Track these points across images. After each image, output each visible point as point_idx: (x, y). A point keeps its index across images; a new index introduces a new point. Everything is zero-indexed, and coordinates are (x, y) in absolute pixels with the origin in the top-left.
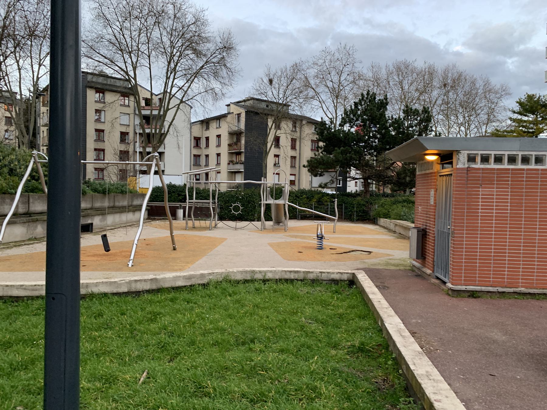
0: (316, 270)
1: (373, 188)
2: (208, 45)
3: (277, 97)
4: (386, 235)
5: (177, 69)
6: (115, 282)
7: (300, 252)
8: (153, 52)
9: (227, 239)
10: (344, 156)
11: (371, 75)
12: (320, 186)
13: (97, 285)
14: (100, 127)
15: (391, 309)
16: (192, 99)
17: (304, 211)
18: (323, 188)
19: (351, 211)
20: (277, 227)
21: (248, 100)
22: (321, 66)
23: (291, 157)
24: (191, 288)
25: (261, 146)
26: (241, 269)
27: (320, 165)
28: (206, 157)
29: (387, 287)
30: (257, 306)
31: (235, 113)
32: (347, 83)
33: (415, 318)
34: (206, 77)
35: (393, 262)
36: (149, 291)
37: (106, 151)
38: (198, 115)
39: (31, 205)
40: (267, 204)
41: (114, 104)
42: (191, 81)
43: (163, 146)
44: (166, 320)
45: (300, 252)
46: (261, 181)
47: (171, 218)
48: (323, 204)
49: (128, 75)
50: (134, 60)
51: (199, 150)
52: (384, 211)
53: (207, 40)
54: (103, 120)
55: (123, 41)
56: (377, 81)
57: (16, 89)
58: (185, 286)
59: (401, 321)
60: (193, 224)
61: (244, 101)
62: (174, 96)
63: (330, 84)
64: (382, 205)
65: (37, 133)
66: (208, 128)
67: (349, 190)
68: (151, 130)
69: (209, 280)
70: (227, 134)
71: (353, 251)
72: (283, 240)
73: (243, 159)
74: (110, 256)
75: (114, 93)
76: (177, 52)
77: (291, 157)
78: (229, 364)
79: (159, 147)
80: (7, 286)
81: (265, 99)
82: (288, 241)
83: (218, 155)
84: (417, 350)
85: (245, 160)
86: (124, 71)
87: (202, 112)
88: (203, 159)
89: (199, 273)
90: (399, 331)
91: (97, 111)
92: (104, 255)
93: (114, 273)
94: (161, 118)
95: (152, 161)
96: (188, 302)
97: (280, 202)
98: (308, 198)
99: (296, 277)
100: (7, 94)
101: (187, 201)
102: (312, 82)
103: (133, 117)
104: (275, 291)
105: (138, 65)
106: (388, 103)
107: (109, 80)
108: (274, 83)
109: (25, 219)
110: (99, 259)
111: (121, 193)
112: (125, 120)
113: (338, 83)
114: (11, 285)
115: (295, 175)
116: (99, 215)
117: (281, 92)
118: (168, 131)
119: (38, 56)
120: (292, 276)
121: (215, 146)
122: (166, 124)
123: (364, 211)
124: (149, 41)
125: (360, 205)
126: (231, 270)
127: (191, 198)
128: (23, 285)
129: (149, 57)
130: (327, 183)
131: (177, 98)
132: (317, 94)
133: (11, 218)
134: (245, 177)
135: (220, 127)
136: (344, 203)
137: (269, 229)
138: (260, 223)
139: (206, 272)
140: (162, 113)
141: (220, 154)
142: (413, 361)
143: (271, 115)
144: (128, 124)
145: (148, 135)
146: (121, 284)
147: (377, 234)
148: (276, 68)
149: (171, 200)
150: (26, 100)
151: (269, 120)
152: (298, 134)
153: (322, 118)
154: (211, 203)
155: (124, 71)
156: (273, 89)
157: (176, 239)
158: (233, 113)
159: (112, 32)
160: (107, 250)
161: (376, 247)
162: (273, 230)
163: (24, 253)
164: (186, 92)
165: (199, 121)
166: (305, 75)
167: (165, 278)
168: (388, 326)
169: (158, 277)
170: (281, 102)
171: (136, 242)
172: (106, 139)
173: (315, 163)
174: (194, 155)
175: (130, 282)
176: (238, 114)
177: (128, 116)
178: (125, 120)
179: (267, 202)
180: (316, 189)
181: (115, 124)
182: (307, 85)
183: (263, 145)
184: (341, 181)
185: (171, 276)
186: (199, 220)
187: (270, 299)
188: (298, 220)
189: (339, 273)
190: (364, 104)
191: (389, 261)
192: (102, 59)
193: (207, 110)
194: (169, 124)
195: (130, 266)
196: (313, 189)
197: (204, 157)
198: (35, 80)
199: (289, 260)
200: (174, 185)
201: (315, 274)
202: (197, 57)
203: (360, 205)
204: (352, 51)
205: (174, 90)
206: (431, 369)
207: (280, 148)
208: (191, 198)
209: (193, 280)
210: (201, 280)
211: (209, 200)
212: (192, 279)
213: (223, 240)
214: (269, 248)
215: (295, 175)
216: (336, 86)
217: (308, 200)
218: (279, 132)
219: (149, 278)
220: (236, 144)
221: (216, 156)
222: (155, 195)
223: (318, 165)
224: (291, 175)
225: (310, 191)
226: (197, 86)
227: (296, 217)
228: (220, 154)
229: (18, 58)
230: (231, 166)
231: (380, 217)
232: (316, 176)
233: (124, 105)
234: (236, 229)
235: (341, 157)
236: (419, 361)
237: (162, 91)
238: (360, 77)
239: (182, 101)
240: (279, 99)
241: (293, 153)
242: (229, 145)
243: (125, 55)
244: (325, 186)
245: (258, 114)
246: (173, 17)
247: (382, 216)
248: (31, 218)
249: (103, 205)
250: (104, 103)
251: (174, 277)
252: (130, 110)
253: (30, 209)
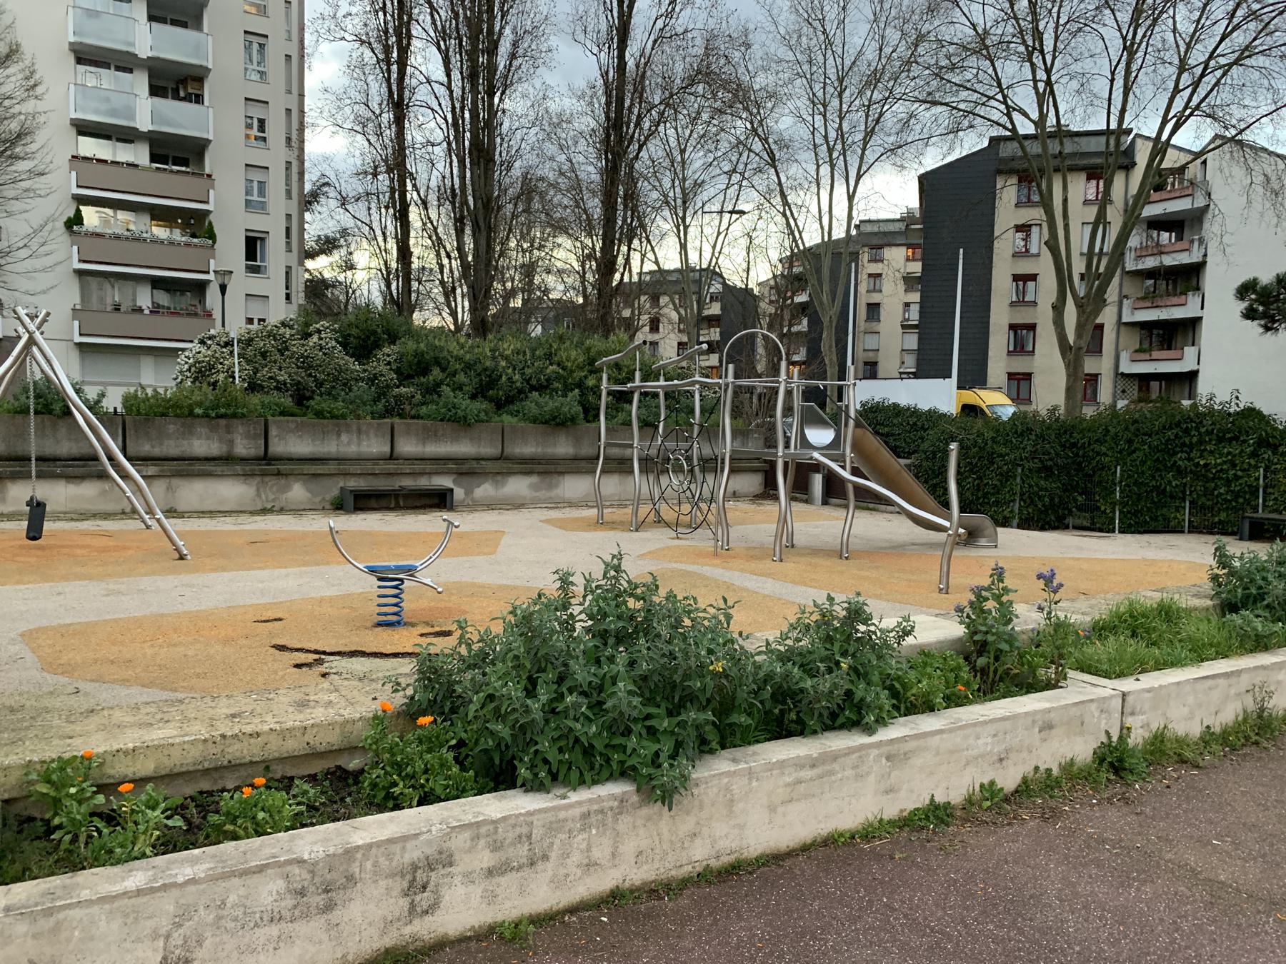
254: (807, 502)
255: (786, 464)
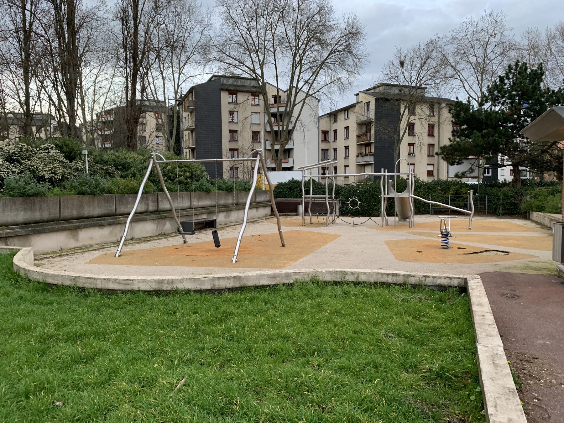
0: (419, 274)
1: (527, 176)
2: (333, 33)
3: (409, 80)
4: (536, 231)
5: (303, 62)
6: (198, 278)
7: (419, 252)
8: (278, 48)
9: (341, 236)
10: (485, 139)
11: (526, 42)
12: (457, 176)
13: (181, 281)
14: (234, 127)
15: (495, 326)
16: (318, 91)
17: (438, 205)
18: (461, 178)
19: (495, 204)
20: (402, 223)
21: (378, 87)
22: (461, 39)
24: (274, 288)
25: (392, 135)
26: (331, 270)
27: (455, 151)
29: (518, 296)
30: (337, 313)
31: (363, 102)
32: (494, 56)
33: (543, 339)
34: (332, 66)
35: (534, 265)
36: (231, 290)
37: (239, 151)
38: (325, 108)
39: (160, 203)
41: (244, 104)
42: (316, 73)
43: (290, 142)
44: (232, 322)
45: (419, 252)
47: (278, 214)
48: (462, 197)
49: (255, 73)
50: (261, 59)
51: (327, 144)
52: (537, 203)
53: (332, 28)
54: (236, 121)
55: (250, 41)
56: (533, 49)
57: (161, 98)
59: (502, 344)
60: (311, 220)
61: (374, 88)
62: (300, 90)
63: (473, 59)
64: (535, 196)
65: (181, 137)
66: (336, 121)
67: (501, 179)
68: (279, 128)
70: (355, 125)
71: (486, 251)
72: (404, 238)
73: (373, 150)
74: (219, 252)
75: (244, 94)
76: (302, 45)
78: (274, 378)
79: (287, 143)
80: (104, 279)
81: (396, 83)
82: (409, 238)
83: (347, 148)
84: (508, 386)
85: (375, 151)
86: (251, 70)
87: (328, 104)
88: (331, 153)
90: (493, 358)
91: (231, 113)
92: (215, 251)
94: (289, 114)
95: (256, 157)
96: (266, 303)
97: (404, 195)
98: (442, 190)
99: (395, 281)
100: (154, 104)
101: (303, 196)
102: (451, 60)
104: (366, 296)
105: (265, 62)
106: (544, 73)
107: (239, 81)
108: (405, 65)
109: (154, 216)
111: (244, 190)
112: (256, 119)
113: (484, 57)
114: (108, 279)
115: (433, 165)
116: (223, 212)
117: (414, 73)
118: (294, 127)
119: (178, 66)
120: (390, 280)
121: (344, 138)
122: (293, 119)
123: (512, 204)
124: (273, 37)
125: (507, 196)
126: (319, 270)
127: (307, 193)
128: (117, 279)
129: (274, 53)
130: (465, 172)
131: (303, 92)
132: (457, 71)
133: (133, 216)
135: (348, 118)
136: (487, 194)
137: (392, 226)
138: (380, 218)
139: (292, 271)
140: (288, 110)
142: (495, 402)
143: (403, 100)
145: (276, 132)
146: (204, 281)
147: (524, 231)
148: (407, 49)
149: (293, 196)
151: (402, 106)
152: (437, 118)
153: (457, 98)
154: (327, 198)
155: (251, 70)
156: (404, 71)
157: (284, 236)
158: (362, 102)
159: (239, 33)
161: (518, 246)
162: (396, 226)
163: (148, 248)
164: (312, 84)
165: (328, 114)
166: (443, 52)
168: (480, 349)
169: (241, 275)
170: (414, 84)
171: (240, 238)
173: (449, 150)
174: (322, 150)
175: (213, 279)
176: (367, 103)
177: (258, 114)
178: (256, 119)
180: (454, 179)
181: (245, 124)
182: (444, 62)
183: (394, 133)
184: (490, 170)
185: (255, 274)
186: (317, 216)
188: (431, 215)
189: (447, 277)
190: (512, 78)
191: (529, 263)
192: (231, 61)
193: (333, 101)
194: (295, 119)
195: (234, 262)
196: (450, 180)
197: (333, 151)
200: (297, 180)
202: (322, 47)
203: (507, 196)
204: (500, 18)
205: (301, 84)
206: (518, 416)
207: (415, 135)
208: (307, 193)
210: (287, 279)
212: (277, 278)
213: (336, 237)
214: (386, 246)
215: (433, 165)
216: (480, 60)
217: (443, 192)
218: (412, 117)
219: (232, 276)
220: (365, 134)
221: (344, 149)
222: (279, 191)
223: (453, 151)
224: (428, 164)
225: (446, 182)
226: (323, 78)
227: (429, 212)
229: (162, 70)
231: (533, 211)
232: (452, 164)
233: (254, 105)
234: (354, 225)
235: (481, 142)
236: (504, 403)
237: (288, 88)
238: (511, 47)
239: (308, 95)
240: (412, 81)
241: (431, 141)
242: (358, 137)
243: (252, 54)
244: (463, 175)
246: (297, 9)
247: (534, 209)
248: (159, 215)
249: (227, 202)
250: (237, 103)
252: (261, 109)
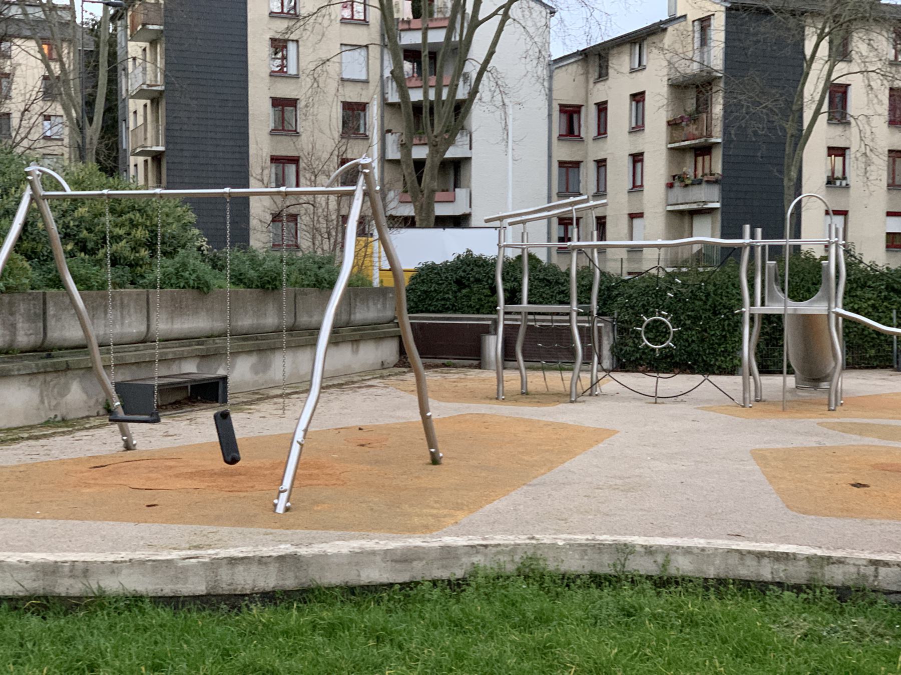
0: (857, 554)
6: (168, 561)
13: (114, 568)
14: (285, 90)
23: (890, 151)
26: (582, 538)
28: (598, 167)
31: (690, 18)
36: (269, 597)
39: (51, 322)
40: (767, 318)
41: (320, 20)
43: (461, 139)
46: (741, 237)
54: (292, 70)
58: (391, 585)
60: (524, 383)
66: (603, 75)
69: (470, 569)
70: (664, 90)
72: (812, 442)
73: (718, 168)
77: (890, 151)
79: (450, 142)
82: (828, 443)
83: (637, 158)
85: (724, 169)
88: (588, 174)
89: (436, 545)
92: (222, 474)
93: (224, 530)
97: (813, 307)
99: (781, 576)
101: (501, 307)
103: (378, 56)
104: (691, 622)
109: (32, 364)
110: (203, 485)
111: (314, 286)
116: (249, 352)
120: (766, 572)
121: (627, 129)
122: (472, 68)
126: (547, 539)
127: (513, 297)
134: (723, 227)
135: (641, 67)
137: (774, 403)
140: (456, 38)
141: (642, 154)
143: (815, 14)
144: (364, 77)
145: (417, 108)
146: (185, 569)
150: (93, 25)
154: (574, 315)
158: (685, 16)
160: (229, 459)
163: (13, 462)
167: (325, 556)
169: (303, 551)
171: (299, 436)
172: (303, 126)
174: (562, 164)
175: (215, 564)
176: (701, 20)
177: (363, 52)
179: (767, 310)
181: (321, 80)
187: (658, 650)
194: (478, 67)
195: (280, 509)
198: (459, 16)
199: (805, 512)
200: (480, 258)
201: (853, 570)
207: (849, 123)
208: (513, 297)
209: (418, 565)
210: (444, 567)
211: (568, 303)
213: (601, 435)
214: (753, 466)
218: (841, 68)
219: (275, 554)
220: (693, 118)
221: (627, 163)
224: (889, 214)
228: (642, 154)
230: (678, 192)
234: (656, 398)
242: (673, 124)
245: (767, 12)
248: (49, 361)
251: (353, 554)
253: (49, 334)
254: (479, 367)
255: (752, 318)
